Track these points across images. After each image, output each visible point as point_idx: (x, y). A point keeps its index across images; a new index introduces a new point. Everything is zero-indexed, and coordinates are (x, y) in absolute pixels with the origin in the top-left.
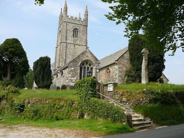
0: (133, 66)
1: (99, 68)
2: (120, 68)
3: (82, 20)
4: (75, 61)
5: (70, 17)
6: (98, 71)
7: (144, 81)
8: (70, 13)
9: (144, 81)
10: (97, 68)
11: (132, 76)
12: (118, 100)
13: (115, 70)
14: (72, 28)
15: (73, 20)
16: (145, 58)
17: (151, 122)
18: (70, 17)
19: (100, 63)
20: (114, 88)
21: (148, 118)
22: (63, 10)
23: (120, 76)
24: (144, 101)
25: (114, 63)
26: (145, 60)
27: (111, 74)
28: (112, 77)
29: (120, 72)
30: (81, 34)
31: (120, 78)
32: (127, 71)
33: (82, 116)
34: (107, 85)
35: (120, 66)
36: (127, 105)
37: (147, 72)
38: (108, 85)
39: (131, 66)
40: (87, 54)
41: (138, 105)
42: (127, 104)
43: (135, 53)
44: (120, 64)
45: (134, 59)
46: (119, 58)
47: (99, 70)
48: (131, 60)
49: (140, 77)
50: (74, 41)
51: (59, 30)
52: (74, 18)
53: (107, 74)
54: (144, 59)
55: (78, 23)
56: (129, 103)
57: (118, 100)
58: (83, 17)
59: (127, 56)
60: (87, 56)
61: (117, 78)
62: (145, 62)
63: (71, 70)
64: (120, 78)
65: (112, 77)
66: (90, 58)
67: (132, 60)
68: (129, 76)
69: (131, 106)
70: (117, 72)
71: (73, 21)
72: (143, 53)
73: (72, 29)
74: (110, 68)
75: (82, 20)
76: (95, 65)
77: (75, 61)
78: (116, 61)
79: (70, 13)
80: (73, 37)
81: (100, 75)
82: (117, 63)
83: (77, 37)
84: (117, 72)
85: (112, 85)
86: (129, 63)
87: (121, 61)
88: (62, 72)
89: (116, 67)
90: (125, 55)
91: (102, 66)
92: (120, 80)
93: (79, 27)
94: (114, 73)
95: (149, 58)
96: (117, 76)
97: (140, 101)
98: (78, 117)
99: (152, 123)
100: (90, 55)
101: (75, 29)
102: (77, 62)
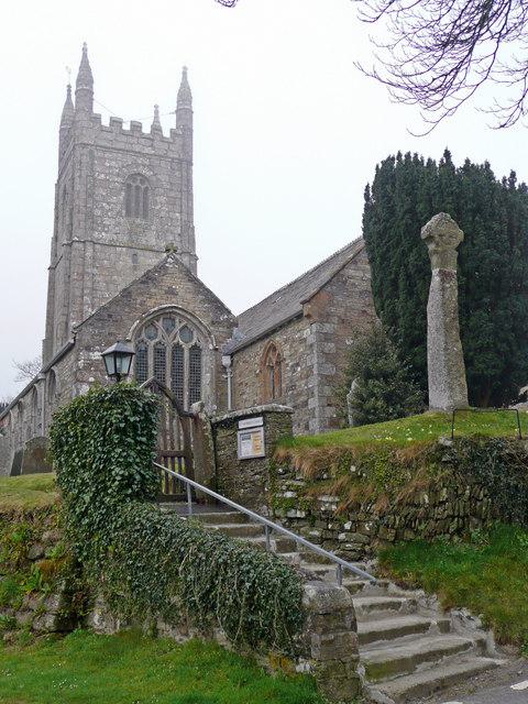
0: (392, 320)
1: (232, 348)
2: (327, 340)
3: (166, 134)
4: (110, 316)
5: (105, 122)
6: (226, 361)
7: (444, 392)
8: (107, 105)
9: (444, 392)
10: (220, 347)
11: (386, 376)
12: (292, 504)
13: (304, 347)
14: (118, 175)
15: (126, 136)
16: (444, 263)
17: (483, 635)
18: (105, 122)
19: (237, 325)
20: (271, 444)
21: (466, 613)
22: (73, 90)
23: (326, 380)
24: (440, 510)
25: (299, 316)
26: (444, 275)
27: (287, 375)
28: (293, 387)
29: (328, 357)
30: (163, 199)
31: (327, 390)
32: (359, 352)
33: (71, 621)
34: (232, 423)
35: (328, 328)
36: (342, 536)
37: (460, 345)
38: (242, 424)
39: (378, 321)
40: (167, 281)
41: (409, 535)
42: (343, 530)
43: (395, 255)
44: (325, 317)
45: (395, 283)
46: (321, 288)
47: (232, 355)
48: (377, 292)
49: (419, 375)
50: (130, 233)
51: (62, 186)
52: (126, 127)
53: (270, 376)
54: (435, 271)
55: (148, 150)
56: (357, 525)
57: (292, 504)
58: (168, 124)
59: (362, 275)
60: (171, 292)
61: (316, 393)
62: (443, 289)
63: (91, 365)
64: (327, 390)
65: (293, 387)
66: (184, 298)
67: (384, 290)
68: (368, 375)
69: (364, 539)
70: (314, 360)
71: (124, 139)
72: (430, 238)
73: (119, 179)
74: (278, 339)
75: (166, 134)
76: (210, 334)
77: (110, 316)
78: (303, 303)
79: (107, 105)
80: (128, 213)
81: (238, 380)
82: (309, 316)
83: (145, 216)
84: (315, 360)
85: (259, 421)
86: (371, 311)
87: (331, 303)
88: (53, 371)
89: (308, 332)
90: (350, 272)
91: (241, 335)
92: (328, 398)
93: (151, 167)
94: (297, 365)
95: (465, 273)
96: (314, 382)
97: (418, 506)
98: (50, 621)
99: (492, 645)
100: (182, 287)
101: (133, 176)
102: (118, 323)
